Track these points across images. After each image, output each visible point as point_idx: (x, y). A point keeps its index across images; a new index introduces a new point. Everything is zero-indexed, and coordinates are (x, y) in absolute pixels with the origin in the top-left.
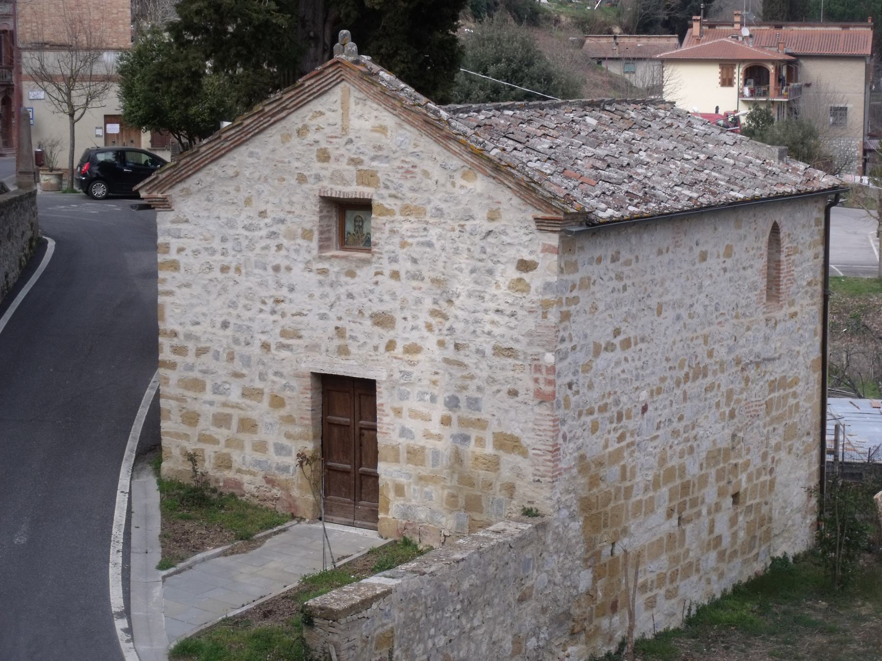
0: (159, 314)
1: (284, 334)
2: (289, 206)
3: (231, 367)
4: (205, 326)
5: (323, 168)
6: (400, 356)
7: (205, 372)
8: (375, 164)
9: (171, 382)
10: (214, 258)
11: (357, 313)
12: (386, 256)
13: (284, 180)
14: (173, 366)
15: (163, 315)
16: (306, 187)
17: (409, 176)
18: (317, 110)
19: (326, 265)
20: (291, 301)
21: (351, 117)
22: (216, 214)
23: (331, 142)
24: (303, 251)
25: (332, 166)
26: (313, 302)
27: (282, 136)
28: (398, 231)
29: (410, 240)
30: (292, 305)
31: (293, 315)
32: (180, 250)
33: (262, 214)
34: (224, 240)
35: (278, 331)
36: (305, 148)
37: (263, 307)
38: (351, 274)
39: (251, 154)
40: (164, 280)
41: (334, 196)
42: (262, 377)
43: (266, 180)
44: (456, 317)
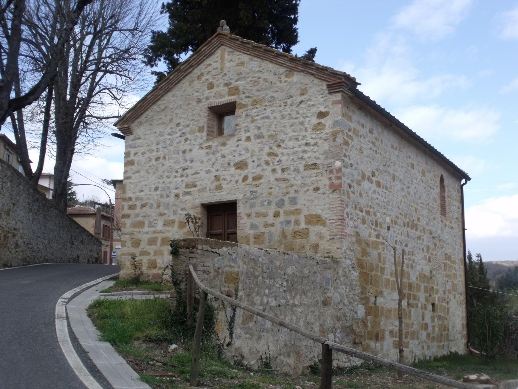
3: (158, 211)
4: (147, 191)
7: (144, 217)
12: (243, 130)
14: (128, 216)
16: (201, 104)
17: (256, 84)
20: (191, 168)
22: (154, 131)
25: (215, 89)
27: (190, 82)
31: (192, 175)
32: (136, 154)
33: (178, 125)
34: (158, 144)
35: (184, 185)
36: (201, 85)
37: (176, 174)
39: (174, 96)
42: (175, 213)
44: (282, 153)
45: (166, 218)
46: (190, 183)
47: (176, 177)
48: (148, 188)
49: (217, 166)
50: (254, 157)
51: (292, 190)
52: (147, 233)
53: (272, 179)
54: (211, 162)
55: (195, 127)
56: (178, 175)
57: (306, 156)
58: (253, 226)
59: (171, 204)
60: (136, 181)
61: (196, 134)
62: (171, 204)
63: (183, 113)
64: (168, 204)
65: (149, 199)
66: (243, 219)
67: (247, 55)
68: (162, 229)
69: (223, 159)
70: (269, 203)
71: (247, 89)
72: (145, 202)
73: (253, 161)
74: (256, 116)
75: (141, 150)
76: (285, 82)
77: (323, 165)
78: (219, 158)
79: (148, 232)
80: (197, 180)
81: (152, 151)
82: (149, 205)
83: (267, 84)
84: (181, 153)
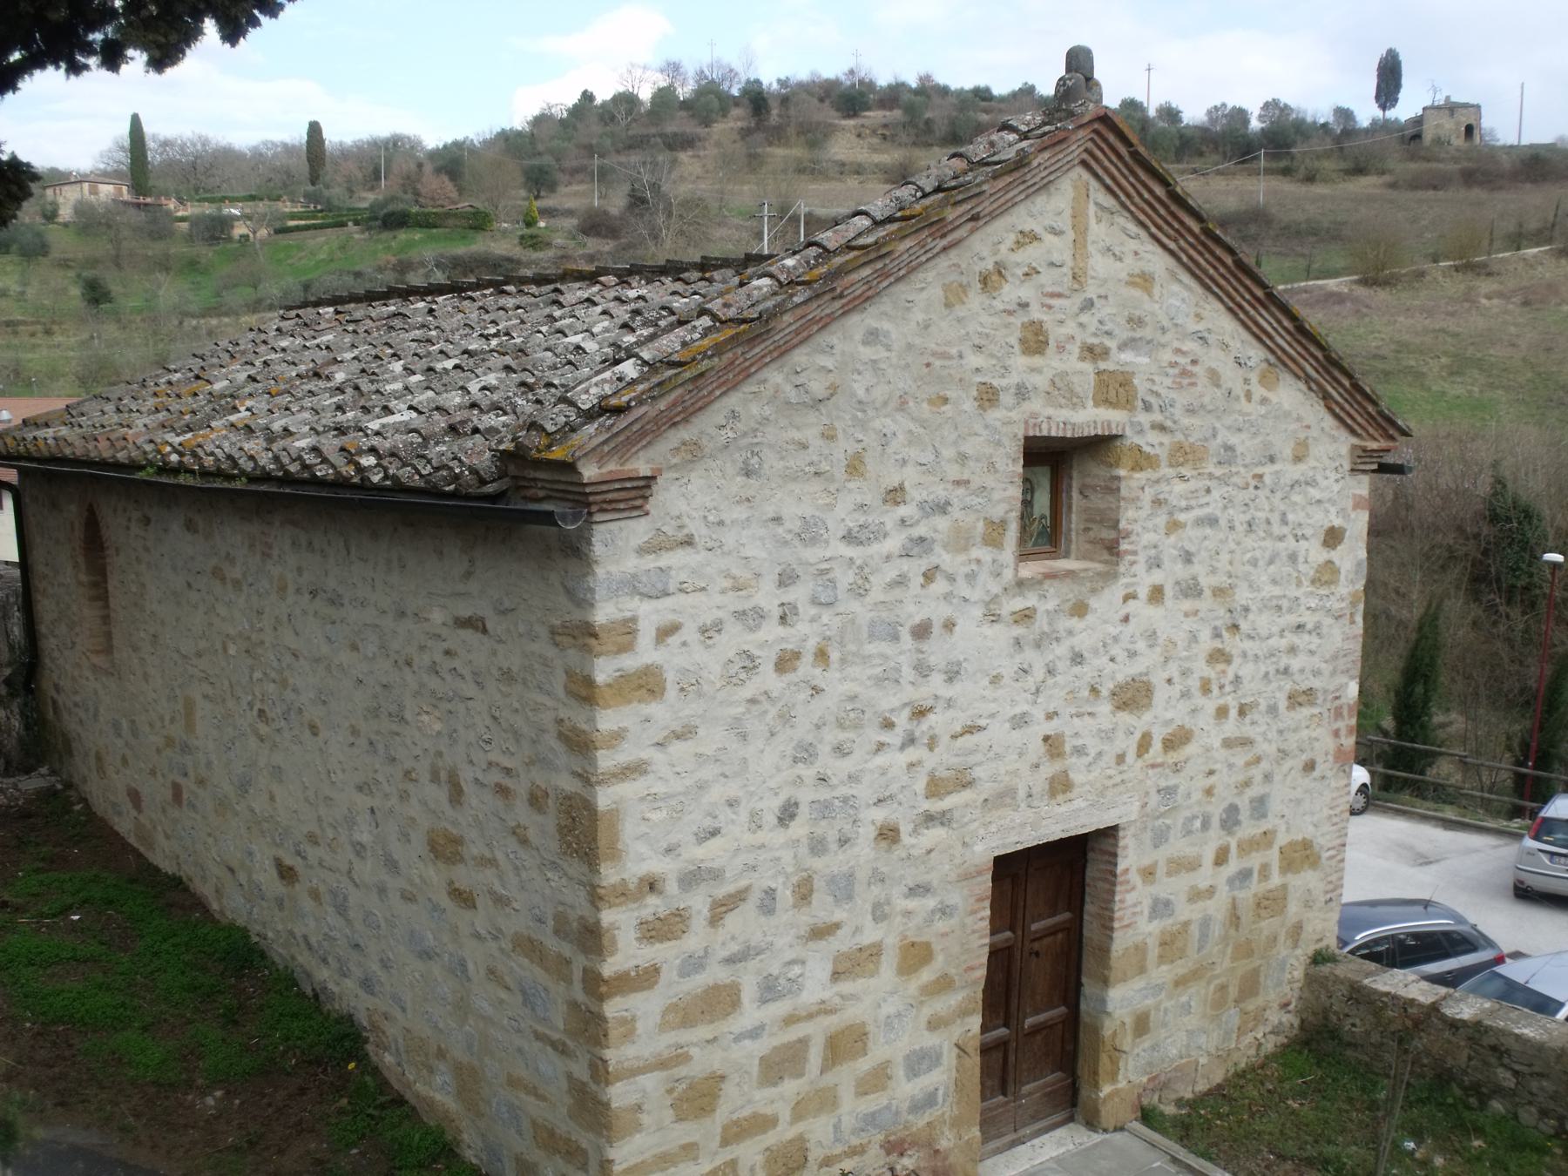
0: (602, 842)
1: (936, 788)
2: (956, 467)
3: (805, 919)
4: (736, 830)
5: (1033, 370)
6: (1159, 760)
7: (730, 961)
8: (1127, 356)
9: (640, 1027)
10: (762, 635)
11: (1086, 693)
12: (1141, 558)
13: (945, 400)
14: (647, 977)
15: (612, 846)
16: (995, 415)
17: (1185, 381)
18: (1027, 228)
19: (1030, 600)
20: (950, 704)
21: (1091, 248)
22: (770, 511)
23: (1050, 307)
24: (983, 576)
25: (1052, 363)
26: (1000, 692)
27: (947, 288)
28: (1166, 500)
29: (1182, 517)
30: (951, 713)
31: (954, 737)
32: (666, 632)
33: (895, 495)
34: (786, 579)
35: (920, 785)
36: (997, 320)
37: (885, 737)
38: (1080, 610)
39: (872, 337)
40: (619, 736)
41: (1053, 434)
42: (880, 913)
43: (902, 406)
44: (1244, 655)
45: (841, 942)
46: (945, 774)
47: (881, 746)
48: (744, 816)
49: (1055, 697)
50: (1171, 664)
51: (1257, 773)
52: (755, 1033)
53: (1217, 743)
54: (1030, 682)
55: (971, 518)
56: (894, 738)
57: (1295, 664)
58: (1161, 908)
59: (862, 875)
60: (677, 785)
61: (976, 552)
62: (862, 875)
63: (913, 439)
64: (850, 877)
65: (754, 868)
66: (1133, 888)
67: (1159, 250)
68: (826, 995)
69: (1077, 670)
70: (1206, 825)
71: (1157, 394)
72: (730, 888)
73: (1169, 681)
74: (1182, 510)
75: (696, 609)
76: (1264, 401)
77: (1325, 691)
78: (1061, 666)
79: (762, 1027)
80: (978, 757)
81: (751, 617)
82: (755, 898)
83: (1218, 393)
84: (905, 634)
